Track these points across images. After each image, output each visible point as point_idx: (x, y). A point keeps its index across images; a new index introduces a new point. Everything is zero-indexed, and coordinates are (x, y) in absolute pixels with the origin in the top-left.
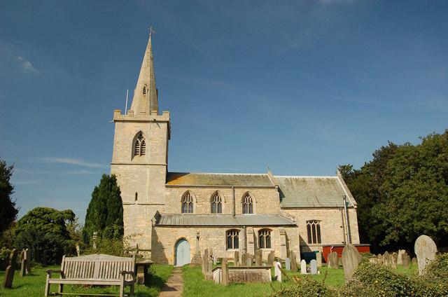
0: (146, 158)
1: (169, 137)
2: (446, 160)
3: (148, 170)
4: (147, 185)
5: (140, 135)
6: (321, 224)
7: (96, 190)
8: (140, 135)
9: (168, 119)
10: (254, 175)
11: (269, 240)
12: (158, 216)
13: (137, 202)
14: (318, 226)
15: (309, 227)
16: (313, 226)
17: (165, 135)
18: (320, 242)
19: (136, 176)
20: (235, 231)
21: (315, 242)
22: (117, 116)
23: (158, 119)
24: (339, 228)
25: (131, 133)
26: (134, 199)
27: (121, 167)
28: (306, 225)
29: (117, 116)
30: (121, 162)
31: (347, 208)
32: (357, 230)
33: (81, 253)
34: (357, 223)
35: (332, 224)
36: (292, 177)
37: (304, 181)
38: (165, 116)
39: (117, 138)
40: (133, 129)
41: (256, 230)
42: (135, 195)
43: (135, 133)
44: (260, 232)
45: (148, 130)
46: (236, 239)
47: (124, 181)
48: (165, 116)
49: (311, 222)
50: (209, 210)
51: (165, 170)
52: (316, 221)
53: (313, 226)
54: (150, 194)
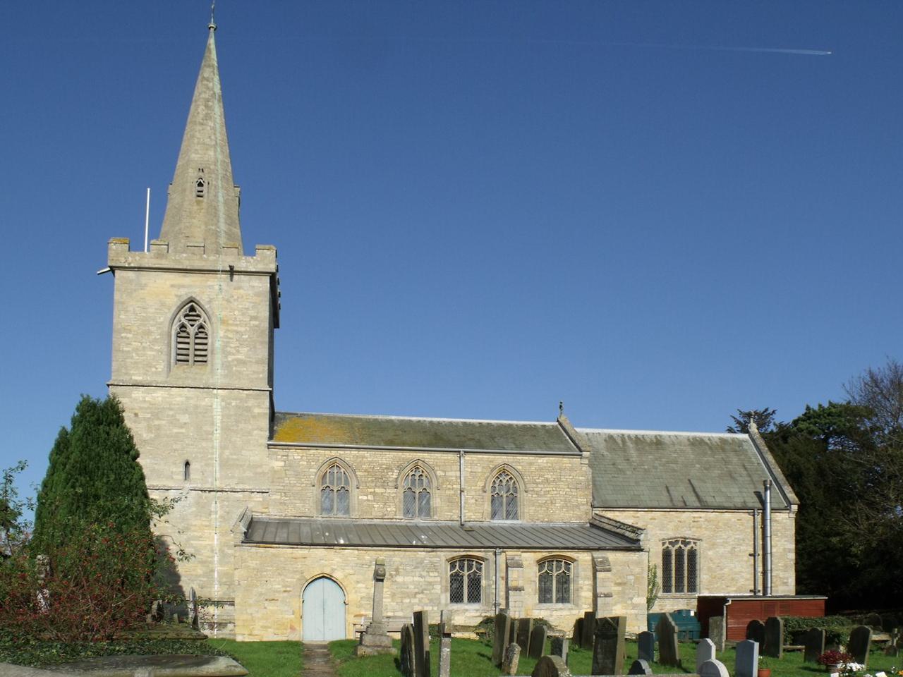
0: (216, 371)
1: (275, 321)
3: (216, 403)
4: (217, 443)
5: (191, 308)
7: (63, 444)
8: (191, 308)
9: (272, 268)
12: (252, 524)
15: (666, 555)
16: (680, 553)
17: (264, 312)
18: (692, 588)
19: (184, 418)
20: (559, 559)
21: (679, 588)
22: (117, 251)
23: (242, 264)
24: (746, 557)
25: (163, 304)
26: (182, 477)
28: (660, 549)
29: (117, 251)
30: (138, 378)
32: (793, 563)
33: (558, 601)
34: (793, 546)
35: (729, 548)
36: (626, 432)
37: (658, 443)
39: (122, 317)
40: (168, 289)
42: (182, 469)
43: (173, 302)
45: (208, 291)
46: (564, 581)
47: (149, 429)
48: (265, 259)
51: (267, 403)
53: (680, 553)
54: (225, 464)
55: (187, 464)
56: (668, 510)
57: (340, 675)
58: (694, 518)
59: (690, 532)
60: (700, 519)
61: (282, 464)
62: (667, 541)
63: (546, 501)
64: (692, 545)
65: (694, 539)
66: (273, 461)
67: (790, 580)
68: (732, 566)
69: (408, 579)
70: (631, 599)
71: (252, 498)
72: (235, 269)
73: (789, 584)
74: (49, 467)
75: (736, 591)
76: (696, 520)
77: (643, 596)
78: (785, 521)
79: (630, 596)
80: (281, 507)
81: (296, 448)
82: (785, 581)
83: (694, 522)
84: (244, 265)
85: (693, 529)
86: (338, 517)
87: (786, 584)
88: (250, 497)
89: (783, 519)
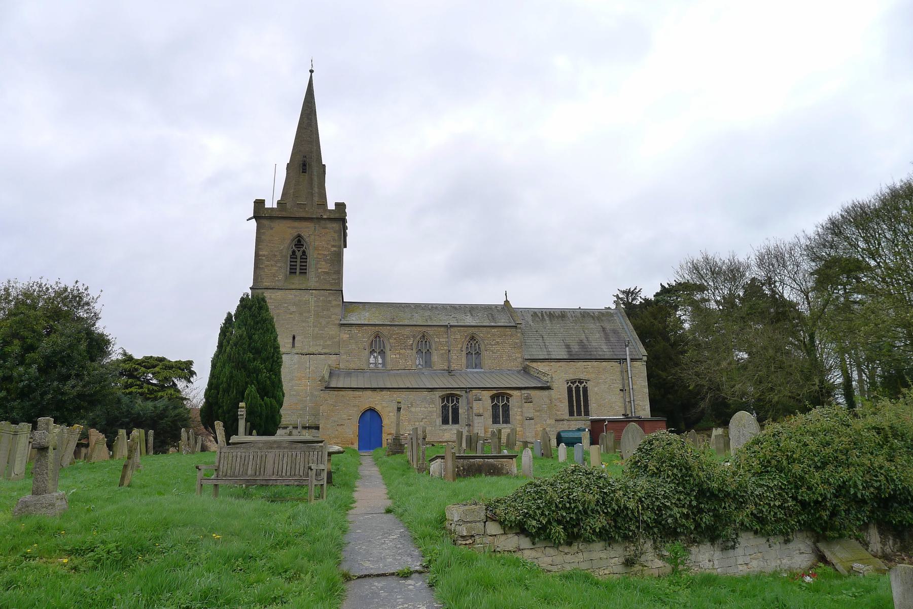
6: (589, 385)
13: (295, 351)
14: (585, 390)
15: (570, 390)
55: (294, 338)
60: (588, 367)
64: (585, 383)
65: (585, 380)
76: (586, 367)
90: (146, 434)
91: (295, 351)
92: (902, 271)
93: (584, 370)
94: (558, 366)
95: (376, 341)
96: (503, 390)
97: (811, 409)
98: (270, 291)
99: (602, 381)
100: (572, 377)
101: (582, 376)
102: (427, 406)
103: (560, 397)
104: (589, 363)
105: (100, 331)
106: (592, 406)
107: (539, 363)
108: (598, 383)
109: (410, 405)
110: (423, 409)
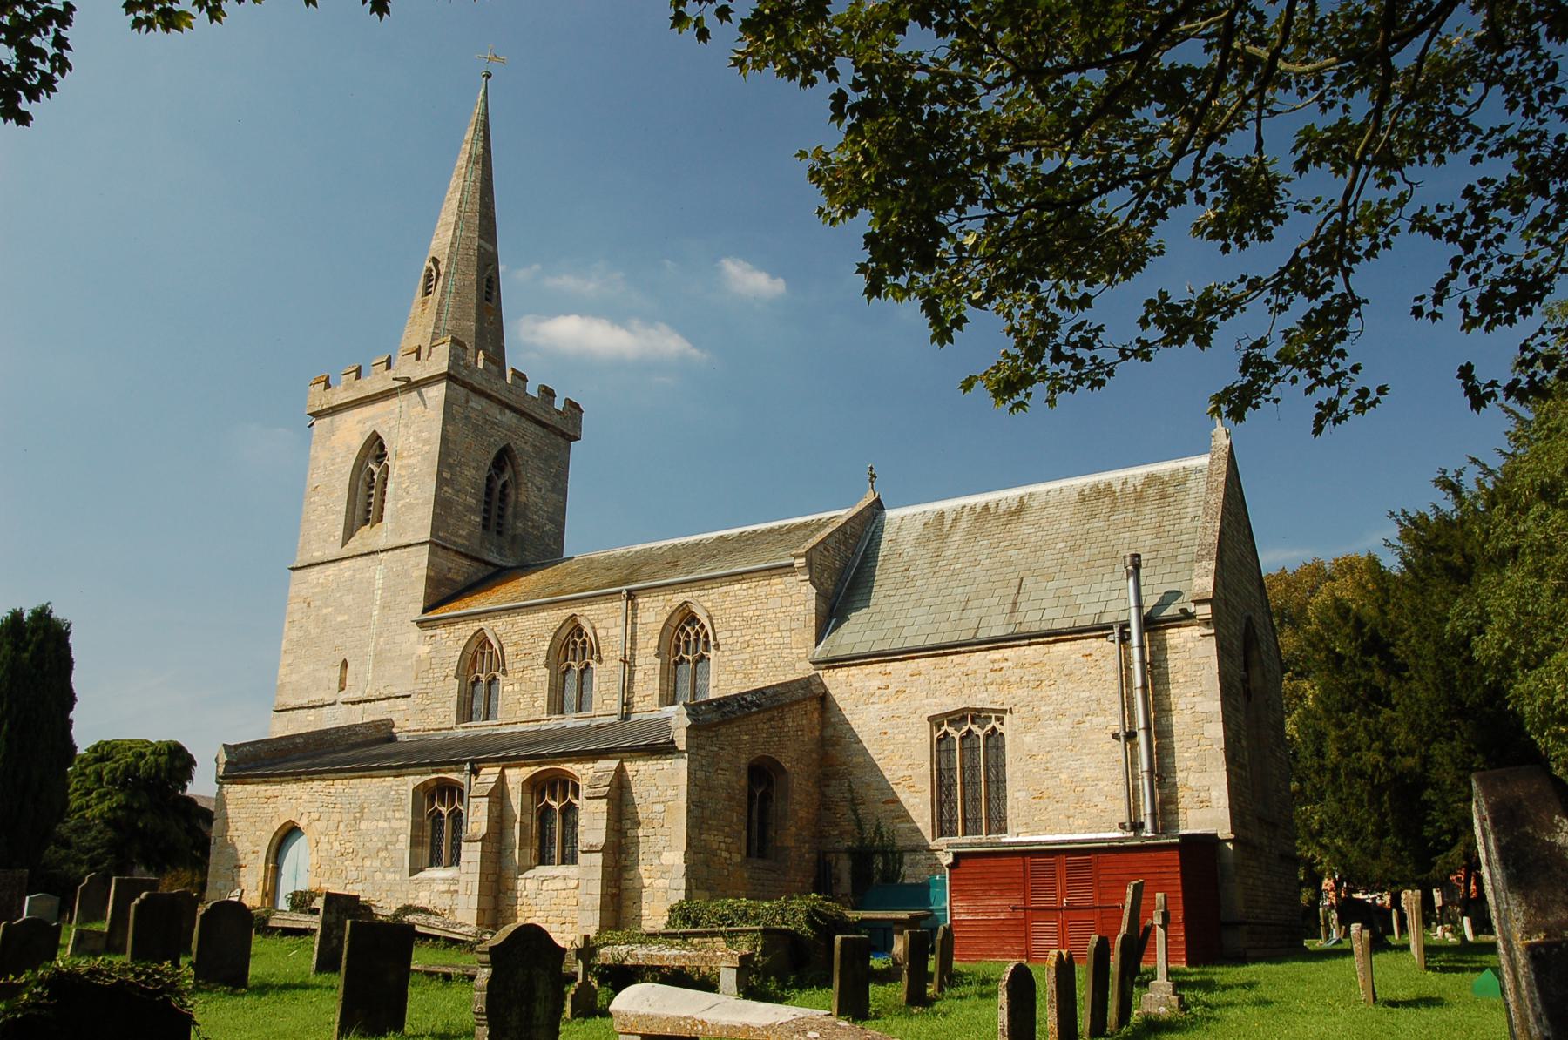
2: (1548, 493)
4: (374, 629)
6: (1007, 728)
10: (736, 531)
11: (1000, 748)
13: (343, 696)
14: (995, 738)
15: (941, 745)
19: (348, 600)
26: (336, 685)
27: (313, 574)
31: (1025, 909)
34: (1216, 706)
35: (1066, 724)
38: (1434, 924)
41: (516, 777)
43: (357, 443)
44: (535, 786)
48: (1434, 924)
49: (957, 717)
50: (542, 701)
52: (978, 715)
55: (345, 664)
56: (941, 652)
57: (1216, 1037)
58: (993, 662)
59: (985, 694)
60: (1005, 664)
61: (428, 649)
62: (993, 716)
63: (744, 660)
64: (994, 723)
65: (994, 711)
66: (421, 646)
67: (1214, 794)
68: (1076, 765)
69: (373, 825)
70: (659, 854)
71: (397, 706)
72: (413, 380)
73: (1214, 803)
74: (857, 610)
75: (1089, 829)
76: (996, 666)
77: (678, 848)
78: (1190, 645)
79: (657, 849)
80: (420, 716)
81: (751, 575)
82: (1203, 795)
83: (992, 671)
84: (418, 372)
85: (992, 688)
86: (478, 728)
87: (1204, 803)
88: (396, 706)
89: (1186, 642)
90: (1024, 862)
91: (343, 696)
92: (952, 155)
93: (991, 676)
94: (909, 672)
95: (483, 654)
96: (553, 763)
97: (1334, 797)
98: (317, 568)
99: (1051, 708)
100: (951, 704)
101: (980, 700)
102: (389, 814)
103: (910, 772)
104: (1008, 653)
105: (1170, 642)
106: (1016, 795)
107: (854, 670)
108: (1037, 718)
109: (358, 815)
110: (382, 824)
